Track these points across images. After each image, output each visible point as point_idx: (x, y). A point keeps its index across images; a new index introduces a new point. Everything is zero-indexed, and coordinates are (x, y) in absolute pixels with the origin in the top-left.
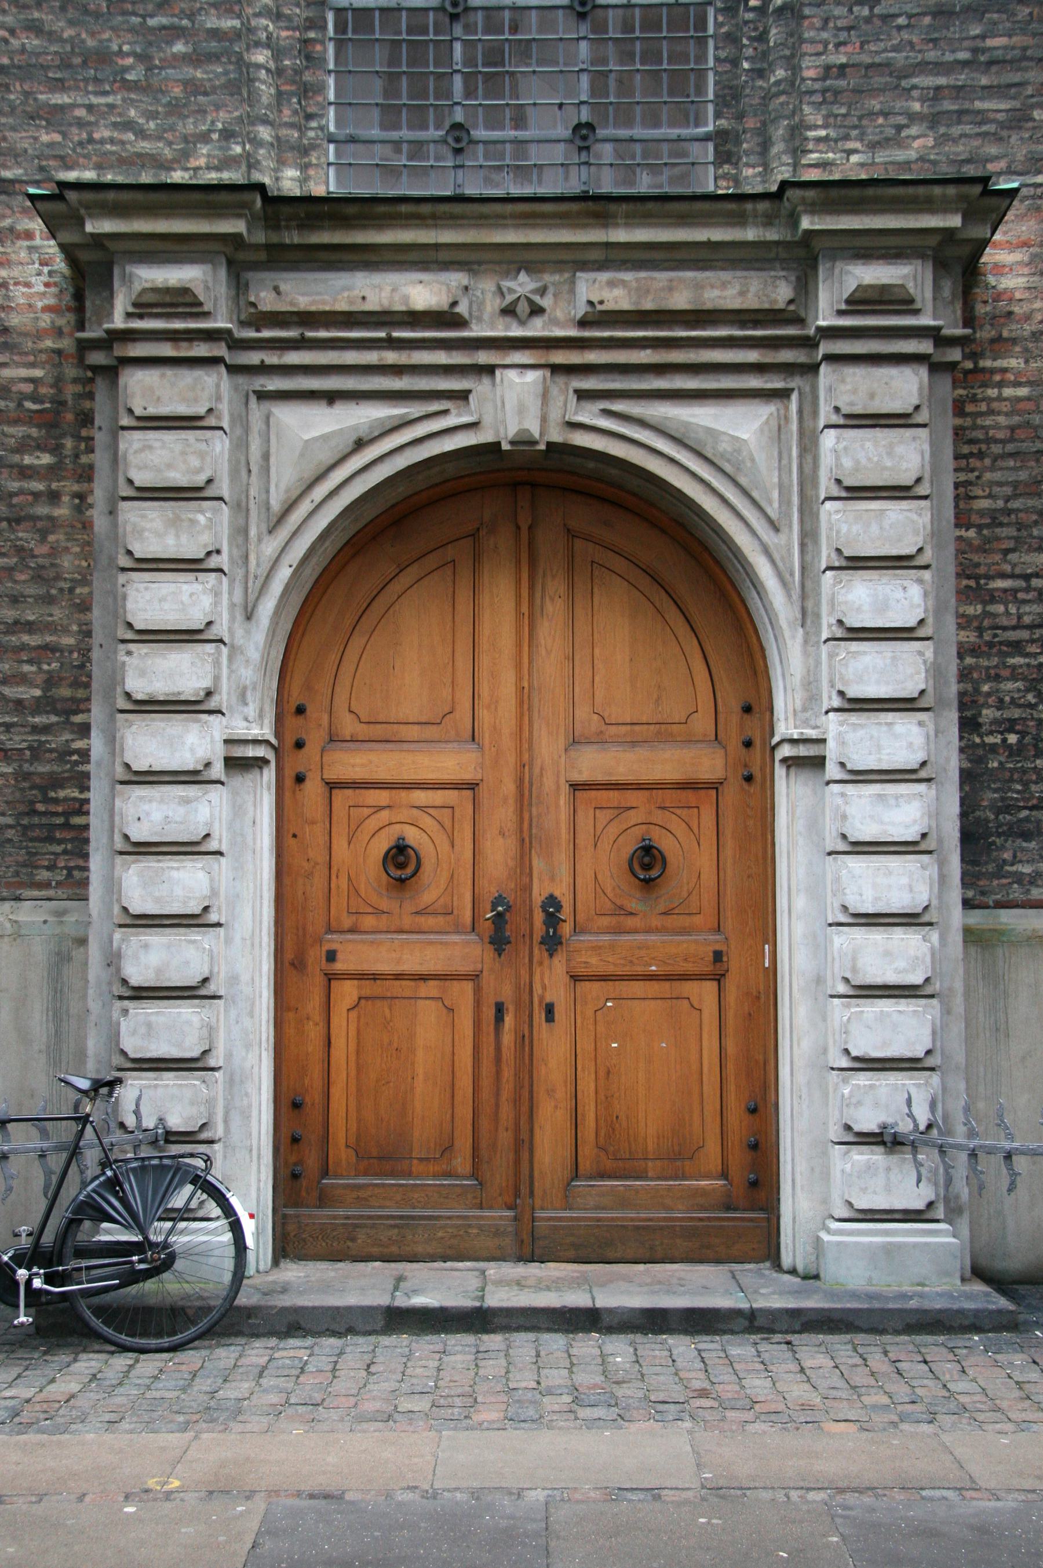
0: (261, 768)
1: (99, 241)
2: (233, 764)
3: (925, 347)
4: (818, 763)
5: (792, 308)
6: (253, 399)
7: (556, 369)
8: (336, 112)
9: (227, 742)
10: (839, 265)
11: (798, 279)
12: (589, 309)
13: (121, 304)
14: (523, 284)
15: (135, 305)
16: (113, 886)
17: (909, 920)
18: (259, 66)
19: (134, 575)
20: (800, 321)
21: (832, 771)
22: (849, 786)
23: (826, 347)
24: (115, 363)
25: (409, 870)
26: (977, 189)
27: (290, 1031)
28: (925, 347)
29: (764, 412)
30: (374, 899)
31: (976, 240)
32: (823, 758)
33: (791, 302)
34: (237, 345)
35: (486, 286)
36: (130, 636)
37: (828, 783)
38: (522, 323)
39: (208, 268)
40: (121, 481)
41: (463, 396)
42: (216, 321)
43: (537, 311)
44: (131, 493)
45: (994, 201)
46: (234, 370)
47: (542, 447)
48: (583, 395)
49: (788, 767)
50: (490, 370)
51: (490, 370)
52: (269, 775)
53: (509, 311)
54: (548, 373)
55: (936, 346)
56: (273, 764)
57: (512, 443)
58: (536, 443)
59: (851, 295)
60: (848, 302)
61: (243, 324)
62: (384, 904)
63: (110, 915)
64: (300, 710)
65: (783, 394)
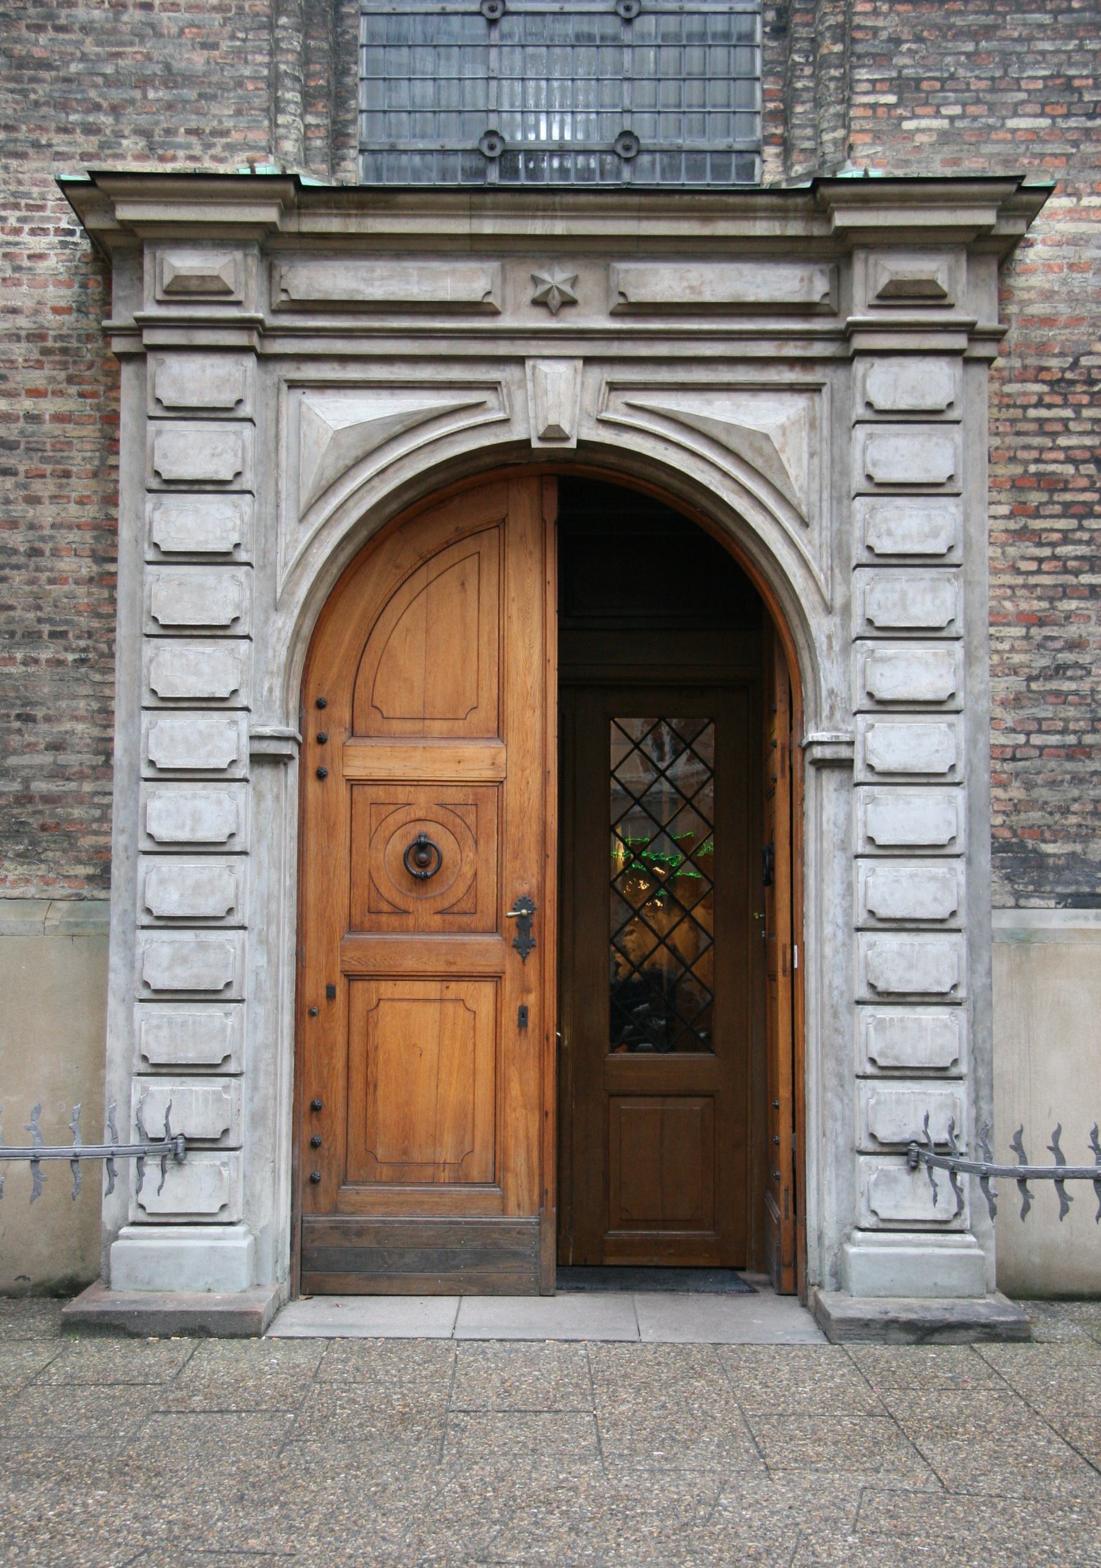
0: (285, 764)
1: (129, 227)
2: (257, 759)
3: (959, 341)
4: (846, 765)
5: (826, 301)
6: (284, 387)
7: (588, 360)
8: (368, 120)
9: (252, 738)
10: (872, 259)
11: (831, 271)
12: (622, 300)
13: (152, 289)
14: (557, 276)
15: (167, 292)
16: (145, 449)
17: (936, 925)
18: (288, 102)
19: (168, 425)
20: (833, 314)
21: (860, 773)
22: (876, 789)
23: (862, 342)
24: (142, 350)
25: (433, 866)
26: (1013, 188)
27: (310, 1039)
28: (959, 341)
29: (797, 405)
30: (398, 900)
31: (1011, 236)
32: (852, 761)
33: (826, 295)
34: (267, 333)
35: (521, 273)
36: (159, 413)
37: (858, 784)
38: (554, 313)
39: (238, 255)
40: (145, 691)
41: (493, 386)
42: (248, 310)
43: (570, 302)
44: (155, 630)
45: (1025, 198)
46: (264, 359)
47: (572, 444)
48: (613, 387)
49: (818, 769)
50: (520, 360)
51: (520, 360)
52: (294, 768)
53: (539, 303)
54: (579, 364)
55: (970, 340)
56: (297, 761)
57: (541, 439)
58: (566, 439)
59: (884, 289)
60: (880, 297)
61: (275, 312)
62: (420, 828)
63: (142, 481)
64: (321, 740)
65: (815, 389)
